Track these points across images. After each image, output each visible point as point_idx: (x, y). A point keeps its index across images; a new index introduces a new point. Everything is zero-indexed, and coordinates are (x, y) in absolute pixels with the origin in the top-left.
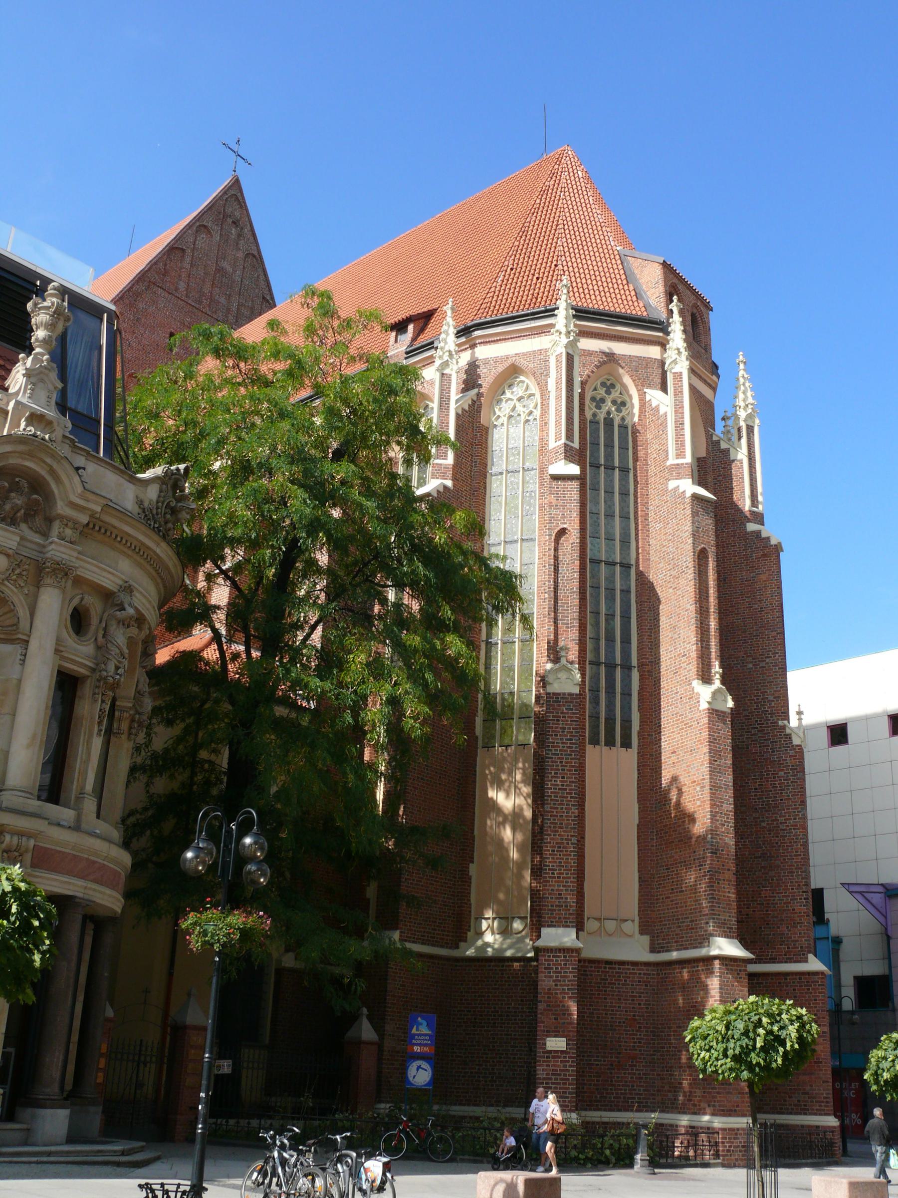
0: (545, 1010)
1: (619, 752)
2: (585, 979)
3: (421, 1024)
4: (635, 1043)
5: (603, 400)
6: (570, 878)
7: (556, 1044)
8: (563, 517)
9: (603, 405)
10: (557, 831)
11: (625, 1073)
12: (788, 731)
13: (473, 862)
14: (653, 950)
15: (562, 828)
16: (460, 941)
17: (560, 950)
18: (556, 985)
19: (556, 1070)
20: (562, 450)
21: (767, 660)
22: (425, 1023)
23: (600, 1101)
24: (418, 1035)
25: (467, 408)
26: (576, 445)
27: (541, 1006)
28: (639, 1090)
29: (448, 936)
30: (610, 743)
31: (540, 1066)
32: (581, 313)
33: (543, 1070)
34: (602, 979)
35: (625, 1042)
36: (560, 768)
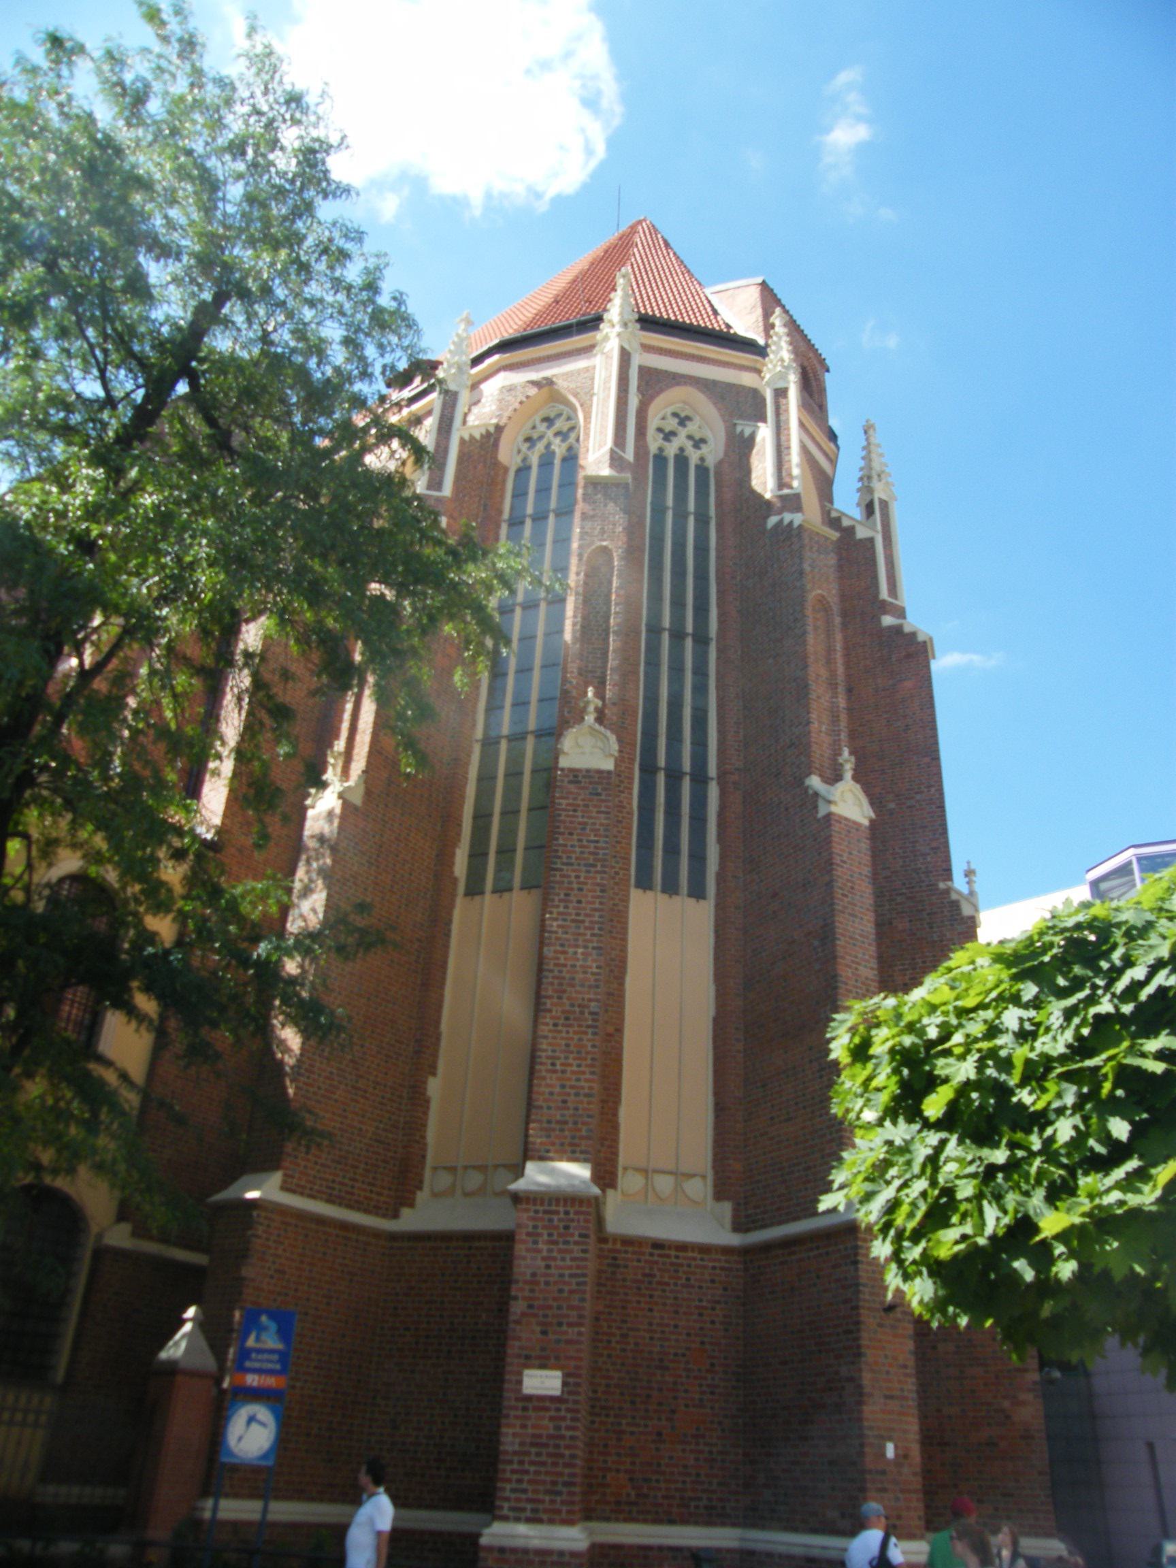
0: (523, 1314)
1: (683, 904)
2: (614, 1273)
3: (265, 1329)
4: (703, 1393)
5: (673, 434)
6: (584, 1073)
7: (542, 1382)
8: (603, 532)
9: (674, 439)
10: (564, 991)
11: (684, 1451)
12: (954, 896)
13: (434, 1074)
14: (738, 1227)
15: (573, 986)
16: (404, 1205)
17: (558, 1200)
18: (548, 1267)
19: (540, 1436)
20: (607, 457)
21: (918, 797)
22: (273, 1327)
23: (635, 1504)
24: (259, 1351)
25: (478, 436)
26: (629, 455)
27: (518, 1308)
28: (710, 1483)
29: (379, 1194)
30: (670, 887)
31: (508, 1426)
32: (648, 322)
33: (514, 1435)
34: (644, 1275)
35: (686, 1391)
36: (575, 886)
